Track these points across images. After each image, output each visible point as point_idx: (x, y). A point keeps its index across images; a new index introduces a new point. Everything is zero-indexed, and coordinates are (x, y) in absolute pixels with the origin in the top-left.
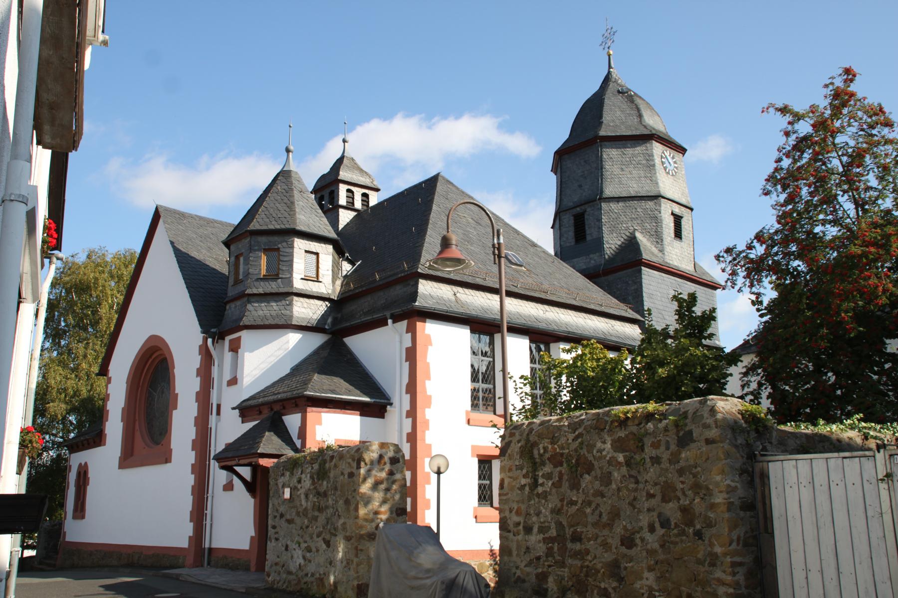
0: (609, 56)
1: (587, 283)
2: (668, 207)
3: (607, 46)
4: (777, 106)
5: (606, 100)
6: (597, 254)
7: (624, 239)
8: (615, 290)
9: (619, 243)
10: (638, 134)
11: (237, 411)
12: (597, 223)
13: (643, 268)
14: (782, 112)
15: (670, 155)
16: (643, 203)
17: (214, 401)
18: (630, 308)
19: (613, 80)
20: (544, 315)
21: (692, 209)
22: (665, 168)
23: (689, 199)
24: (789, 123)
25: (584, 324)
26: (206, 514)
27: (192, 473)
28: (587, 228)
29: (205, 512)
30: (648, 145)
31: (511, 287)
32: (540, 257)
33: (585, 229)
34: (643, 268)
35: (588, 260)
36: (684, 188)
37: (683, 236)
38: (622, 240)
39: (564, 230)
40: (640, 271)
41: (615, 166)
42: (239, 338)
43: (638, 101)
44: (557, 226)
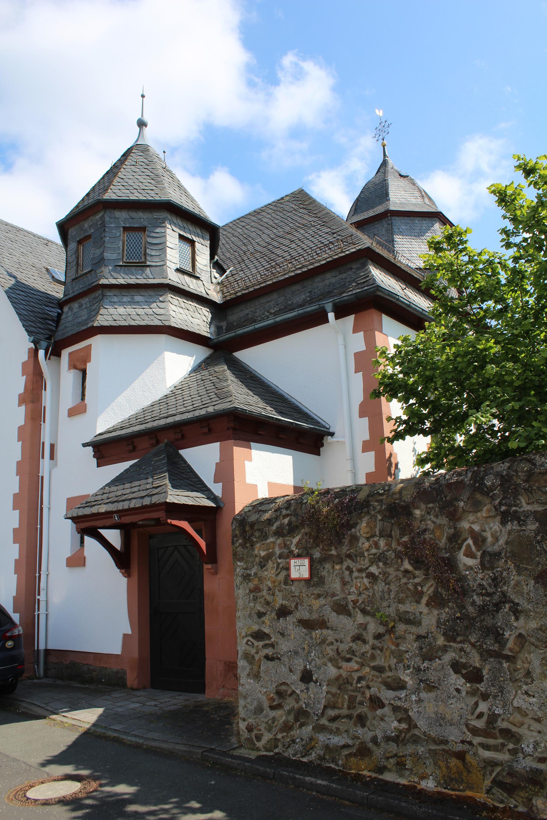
0: (384, 146)
11: (90, 449)
17: (46, 438)
26: (39, 600)
27: (15, 542)
29: (38, 597)
42: (89, 347)
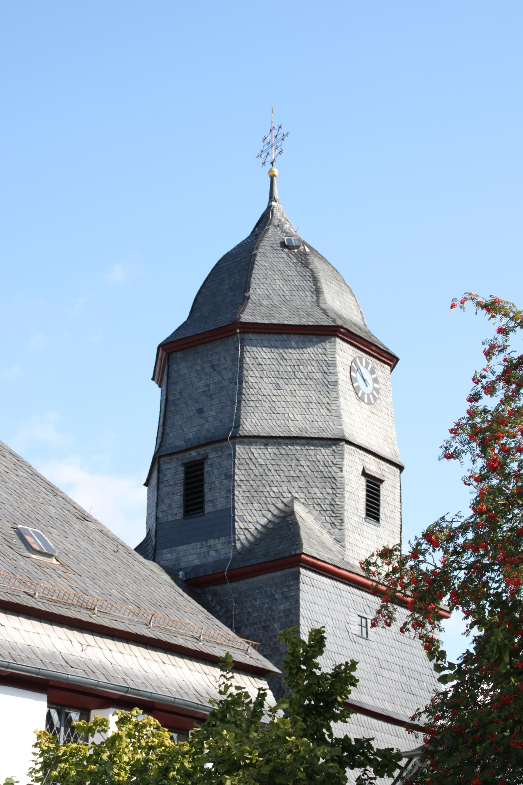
0: (272, 177)
1: (176, 595)
2: (357, 460)
3: (269, 159)
4: (480, 299)
5: (258, 258)
6: (223, 540)
7: (273, 515)
8: (249, 610)
9: (264, 521)
10: (310, 324)
12: (225, 482)
13: (302, 570)
14: (489, 311)
15: (367, 367)
16: (311, 450)
18: (254, 647)
19: (276, 222)
20: (83, 654)
21: (401, 468)
22: (356, 390)
23: (397, 448)
24: (500, 331)
25: (160, 673)
28: (206, 490)
30: (328, 345)
31: (23, 595)
32: (91, 541)
33: (202, 491)
34: (302, 570)
35: (205, 549)
36: (388, 429)
37: (382, 516)
38: (269, 516)
39: (165, 490)
40: (297, 577)
41: (266, 380)
43: (316, 264)
44: (154, 482)
